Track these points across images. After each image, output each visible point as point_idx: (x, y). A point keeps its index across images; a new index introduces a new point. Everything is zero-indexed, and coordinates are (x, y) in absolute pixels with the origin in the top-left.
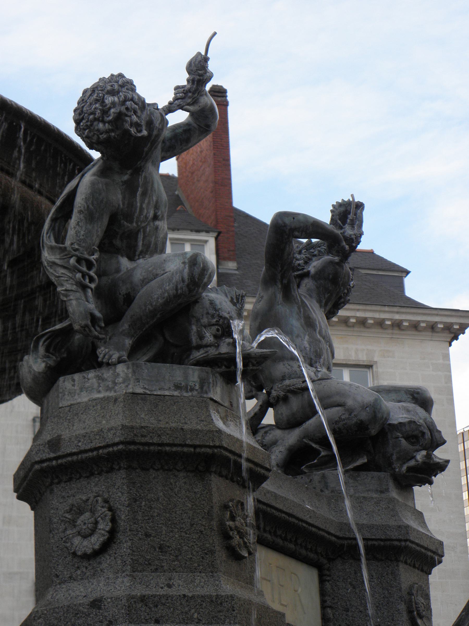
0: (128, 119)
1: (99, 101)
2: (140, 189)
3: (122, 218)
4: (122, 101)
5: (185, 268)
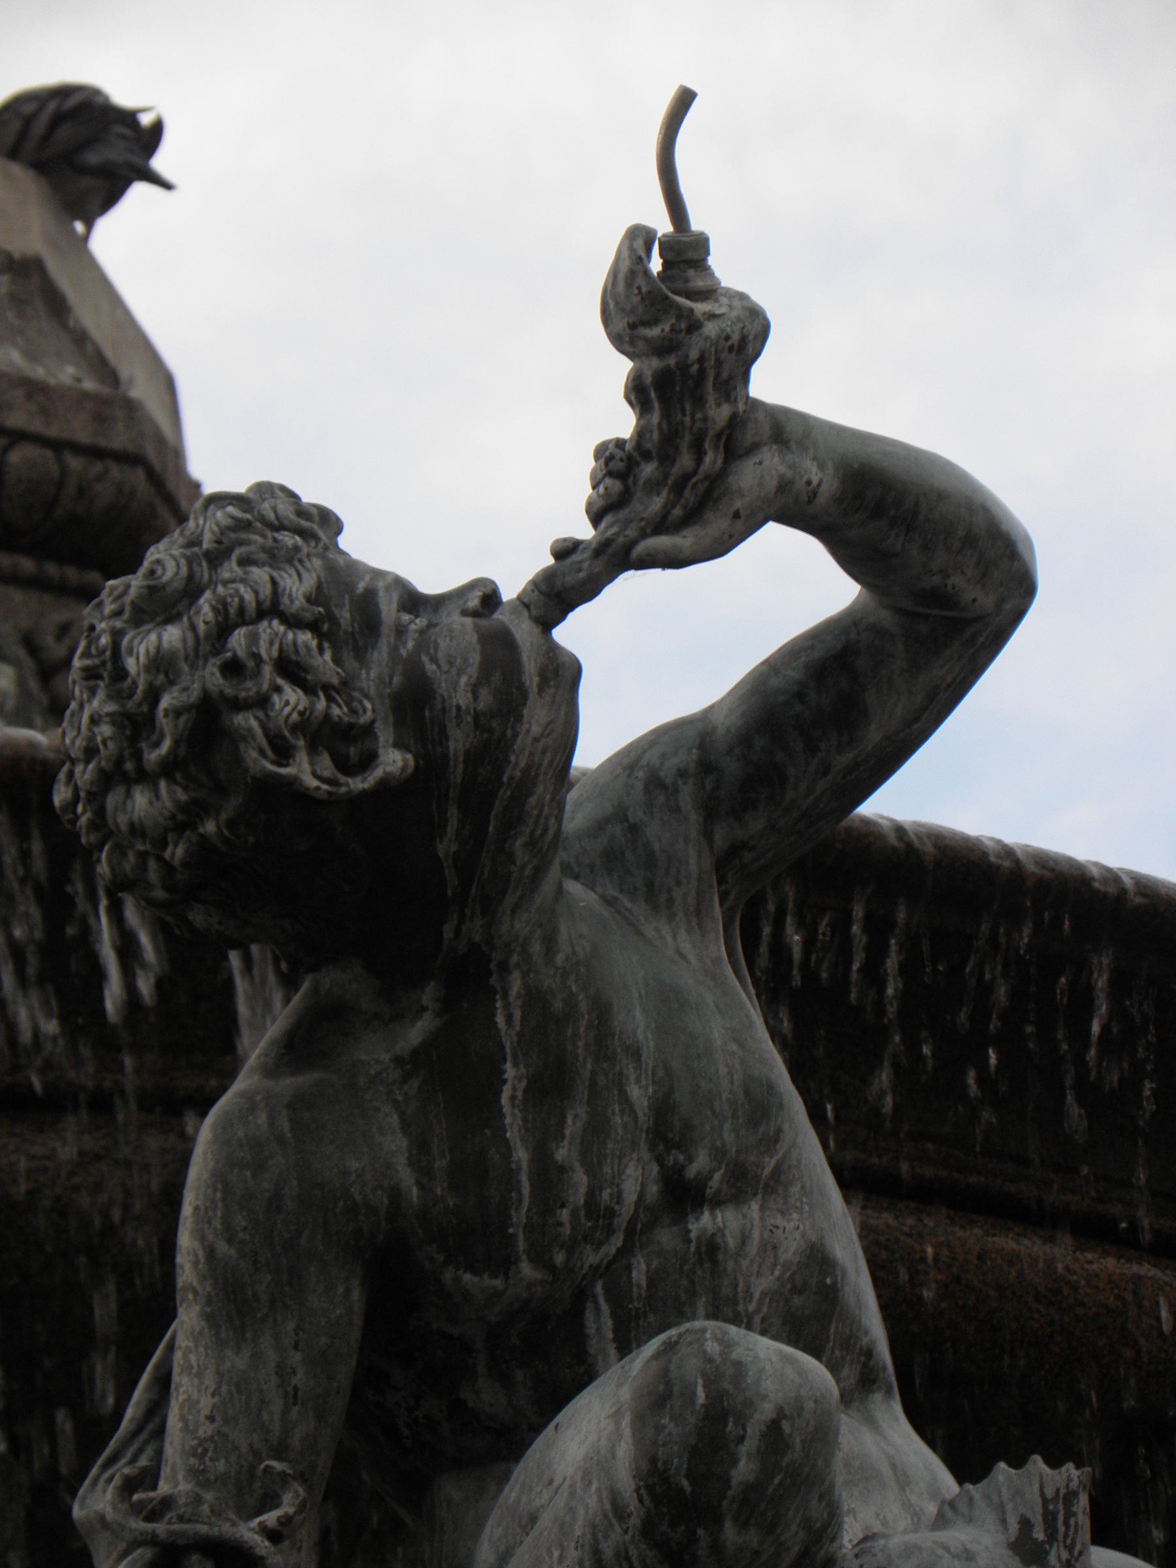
0: (247, 721)
1: (99, 677)
2: (510, 1071)
3: (441, 1258)
4: (208, 636)
5: (620, 1437)
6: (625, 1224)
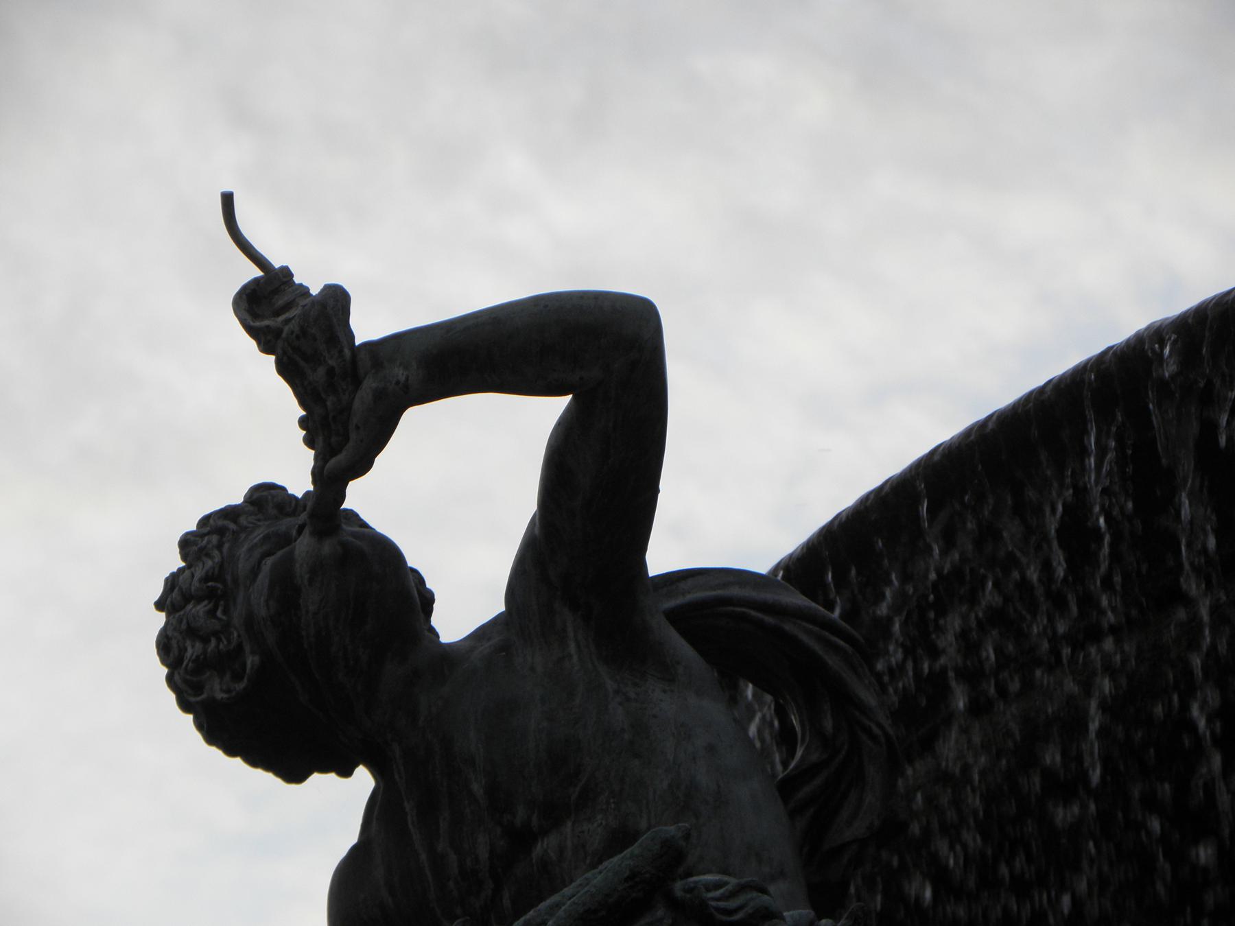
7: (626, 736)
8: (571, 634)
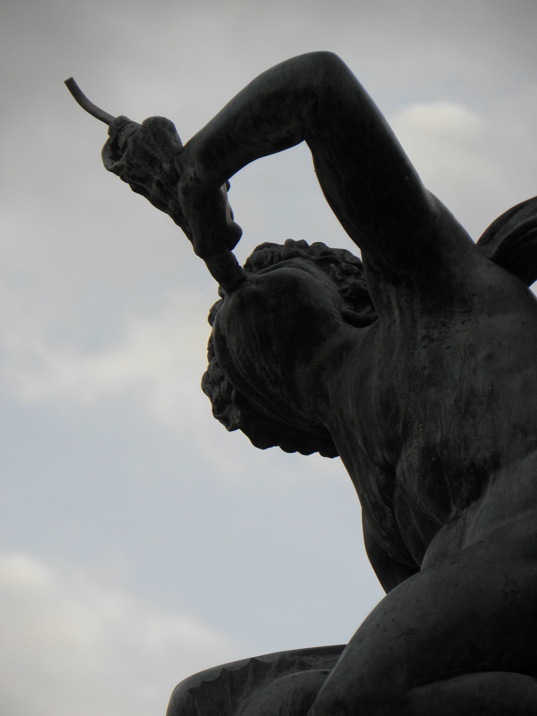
6: (383, 503)
7: (426, 372)
8: (394, 303)
